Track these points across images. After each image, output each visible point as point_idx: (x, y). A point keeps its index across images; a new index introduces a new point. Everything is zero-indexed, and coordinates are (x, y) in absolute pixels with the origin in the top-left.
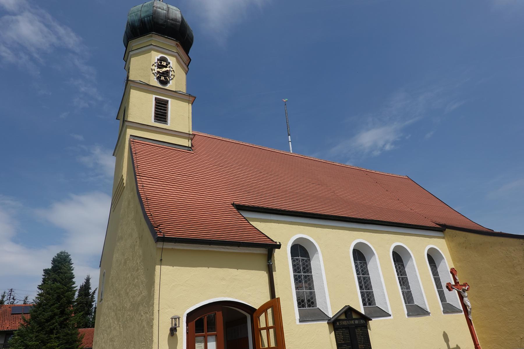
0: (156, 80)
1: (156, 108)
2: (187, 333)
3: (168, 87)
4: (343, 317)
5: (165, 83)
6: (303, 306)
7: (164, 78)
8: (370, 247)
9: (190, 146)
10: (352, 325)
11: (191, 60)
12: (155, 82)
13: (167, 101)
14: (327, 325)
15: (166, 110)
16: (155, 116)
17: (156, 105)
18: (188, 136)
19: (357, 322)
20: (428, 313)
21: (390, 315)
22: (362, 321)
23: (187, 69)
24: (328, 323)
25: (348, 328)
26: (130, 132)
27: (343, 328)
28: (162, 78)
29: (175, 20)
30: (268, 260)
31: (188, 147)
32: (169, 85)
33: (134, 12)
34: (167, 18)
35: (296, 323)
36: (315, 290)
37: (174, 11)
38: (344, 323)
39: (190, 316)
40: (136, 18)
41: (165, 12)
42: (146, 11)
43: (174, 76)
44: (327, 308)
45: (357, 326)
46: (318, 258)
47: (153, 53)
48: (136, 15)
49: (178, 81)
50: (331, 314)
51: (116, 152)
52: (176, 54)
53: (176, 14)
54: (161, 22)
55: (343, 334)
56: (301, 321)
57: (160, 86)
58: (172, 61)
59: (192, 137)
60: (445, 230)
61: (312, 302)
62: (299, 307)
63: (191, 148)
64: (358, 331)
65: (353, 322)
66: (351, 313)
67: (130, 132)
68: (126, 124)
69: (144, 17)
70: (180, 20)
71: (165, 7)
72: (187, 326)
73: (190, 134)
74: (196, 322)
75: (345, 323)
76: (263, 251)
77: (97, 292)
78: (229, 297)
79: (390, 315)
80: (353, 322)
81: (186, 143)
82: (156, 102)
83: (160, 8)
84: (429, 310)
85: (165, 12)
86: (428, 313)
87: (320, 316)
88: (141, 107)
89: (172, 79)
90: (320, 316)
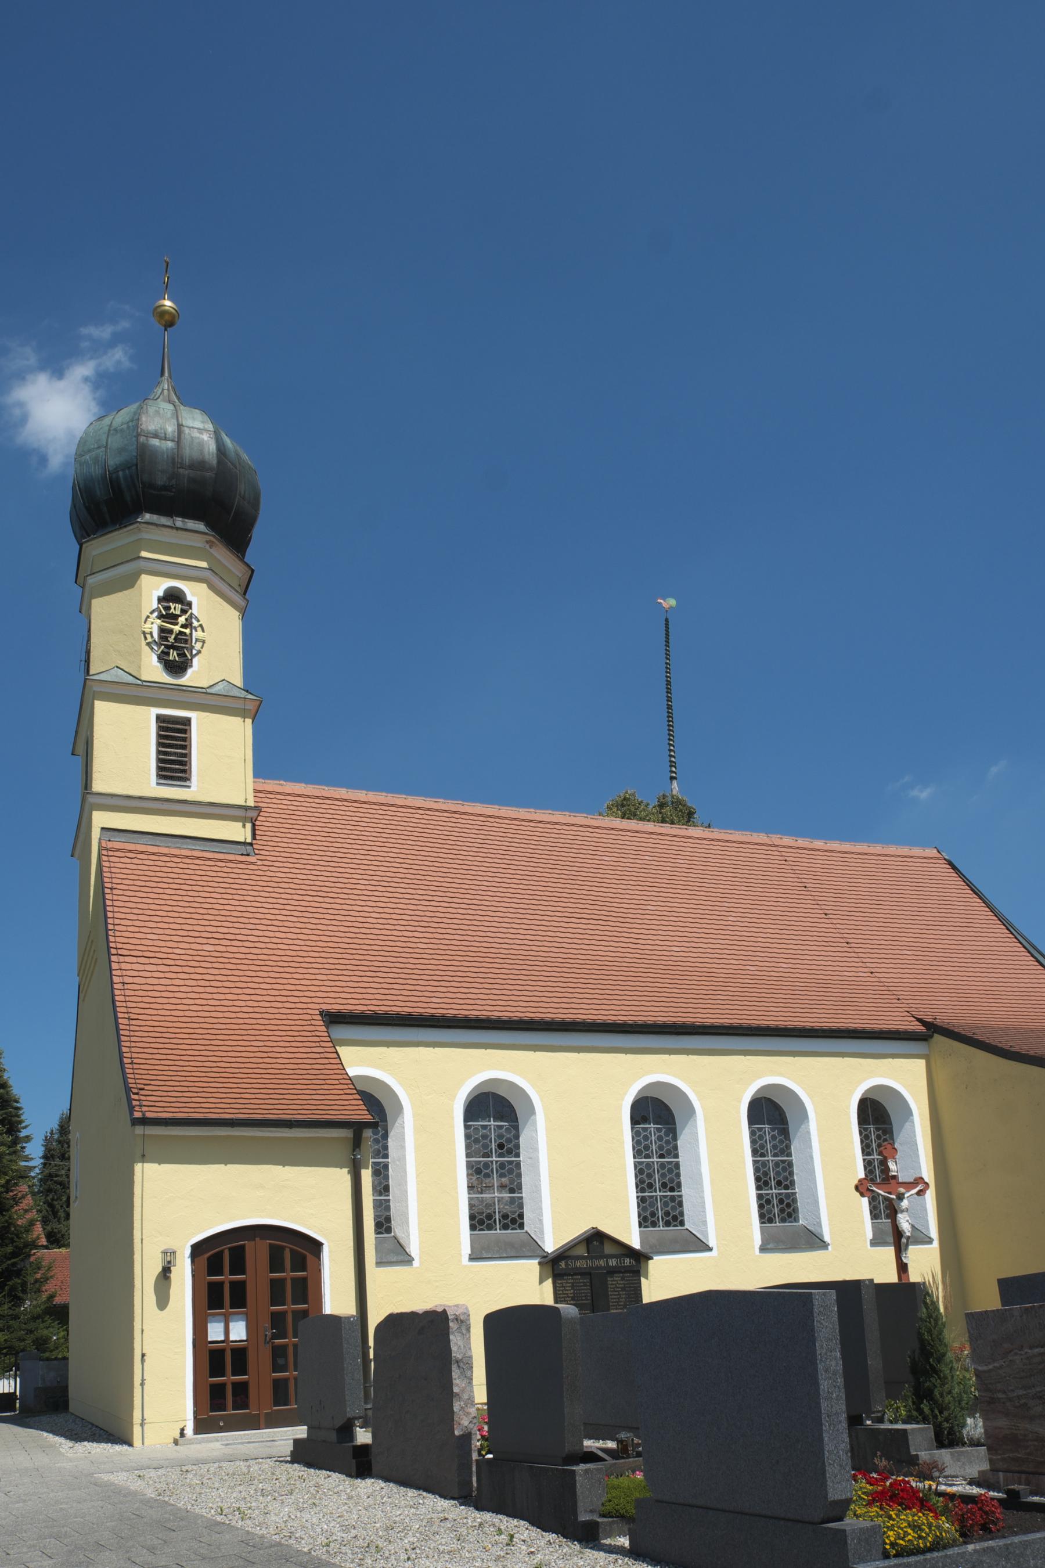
0: (155, 658)
1: (159, 744)
2: (193, 1276)
3: (189, 678)
4: (582, 1251)
5: (177, 667)
6: (770, 1221)
7: (176, 654)
8: (684, 1093)
9: (249, 840)
10: (601, 1268)
11: (253, 571)
12: (152, 669)
13: (187, 721)
14: (538, 1267)
15: (184, 747)
16: (159, 768)
17: (159, 736)
18: (241, 813)
19: (613, 1262)
20: (824, 1245)
21: (711, 1249)
22: (627, 1261)
23: (243, 603)
24: (540, 1263)
25: (590, 1274)
26: (101, 819)
27: (576, 1274)
28: (173, 655)
29: (199, 465)
30: (354, 1150)
31: (244, 843)
32: (190, 671)
33: (90, 451)
34: (175, 460)
35: (460, 1261)
36: (524, 1195)
37: (196, 434)
38: (578, 1264)
39: (198, 1249)
40: (96, 471)
41: (170, 444)
42: (121, 450)
43: (204, 642)
44: (542, 1232)
45: (612, 1272)
46: (535, 1124)
47: (146, 580)
48: (96, 460)
49: (220, 648)
50: (550, 1245)
51: (86, 639)
52: (208, 574)
53: (201, 444)
54: (161, 480)
55: (573, 1287)
56: (472, 1258)
57: (165, 678)
58: (196, 593)
59: (254, 814)
60: (931, 1036)
61: (514, 1220)
62: (377, 1232)
63: (251, 844)
64: (615, 1282)
65: (602, 1263)
66: (602, 1243)
67: (101, 819)
68: (91, 799)
69: (116, 470)
70: (215, 462)
71: (170, 428)
72: (193, 1262)
73: (250, 808)
74: (209, 1259)
75: (582, 1264)
76: (347, 1133)
77: (228, 441)
78: (272, 1217)
79: (711, 1249)
80: (602, 1263)
81: (238, 832)
82: (160, 728)
83: (156, 436)
84: (827, 1238)
85: (170, 444)
86: (824, 1245)
87: (529, 1248)
88: (123, 745)
89: (199, 652)
90: (529, 1248)
